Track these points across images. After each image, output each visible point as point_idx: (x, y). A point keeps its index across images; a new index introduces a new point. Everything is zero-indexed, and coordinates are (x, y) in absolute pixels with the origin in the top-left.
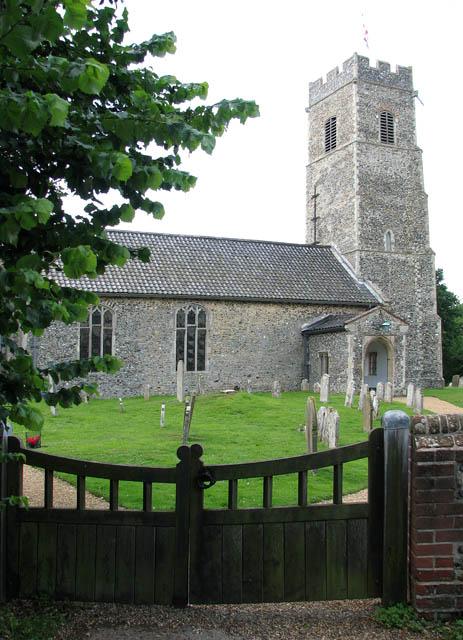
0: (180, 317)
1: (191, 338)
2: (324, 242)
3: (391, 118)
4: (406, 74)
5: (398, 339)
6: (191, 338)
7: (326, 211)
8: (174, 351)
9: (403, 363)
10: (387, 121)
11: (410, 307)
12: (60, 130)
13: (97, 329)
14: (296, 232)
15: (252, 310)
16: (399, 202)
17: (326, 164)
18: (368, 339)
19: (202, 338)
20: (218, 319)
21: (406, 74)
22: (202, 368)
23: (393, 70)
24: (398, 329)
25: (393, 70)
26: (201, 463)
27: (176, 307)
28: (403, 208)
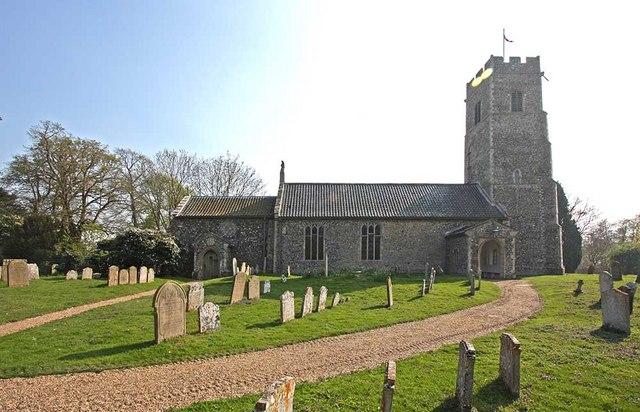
0: (364, 229)
1: (371, 242)
2: (473, 182)
3: (520, 94)
4: (534, 62)
5: (509, 241)
6: (371, 242)
7: (474, 162)
9: (512, 256)
10: (517, 96)
11: (535, 220)
12: (474, 139)
13: (315, 238)
14: (458, 177)
15: (410, 225)
16: (526, 150)
17: (477, 129)
18: (482, 241)
19: (378, 241)
20: (387, 230)
21: (534, 62)
22: (378, 257)
23: (523, 61)
24: (508, 233)
25: (523, 61)
26: (290, 291)
27: (361, 225)
28: (530, 153)
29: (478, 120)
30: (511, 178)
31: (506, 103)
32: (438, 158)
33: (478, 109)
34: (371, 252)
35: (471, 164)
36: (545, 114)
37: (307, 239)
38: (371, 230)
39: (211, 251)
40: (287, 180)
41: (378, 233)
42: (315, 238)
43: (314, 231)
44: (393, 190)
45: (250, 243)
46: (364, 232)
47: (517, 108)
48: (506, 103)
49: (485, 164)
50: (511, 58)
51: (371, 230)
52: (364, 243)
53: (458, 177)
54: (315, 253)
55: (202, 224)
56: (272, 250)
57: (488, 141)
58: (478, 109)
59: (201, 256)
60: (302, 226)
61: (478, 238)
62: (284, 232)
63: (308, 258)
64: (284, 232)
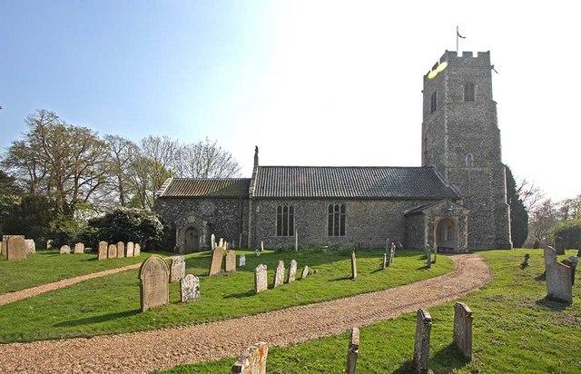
0: (331, 208)
1: (337, 219)
2: (430, 165)
3: (472, 85)
4: (485, 56)
5: (462, 218)
6: (337, 219)
7: (430, 147)
8: (327, 230)
9: (465, 233)
10: (469, 87)
11: (486, 200)
12: (430, 126)
13: (286, 216)
14: (415, 160)
15: (373, 204)
16: (478, 136)
17: (433, 117)
18: (438, 219)
19: (343, 219)
20: (351, 209)
21: (485, 56)
22: (343, 234)
23: (475, 55)
24: (461, 212)
25: (475, 55)
26: (264, 264)
27: (328, 204)
28: (481, 139)
29: (434, 109)
30: (464, 162)
31: (459, 93)
32: (397, 143)
33: (434, 99)
34: (337, 228)
35: (428, 149)
36: (495, 103)
37: (279, 217)
38: (337, 209)
39: (192, 228)
40: (260, 164)
41: (343, 211)
42: (286, 216)
43: (285, 210)
44: (357, 172)
45: (227, 220)
47: (470, 98)
48: (459, 93)
49: (441, 149)
50: (464, 53)
51: (337, 209)
52: (330, 220)
53: (415, 160)
54: (286, 230)
55: (184, 203)
56: (247, 227)
57: (443, 128)
58: (434, 99)
60: (275, 205)
61: (433, 216)
63: (279, 234)
64: (258, 211)
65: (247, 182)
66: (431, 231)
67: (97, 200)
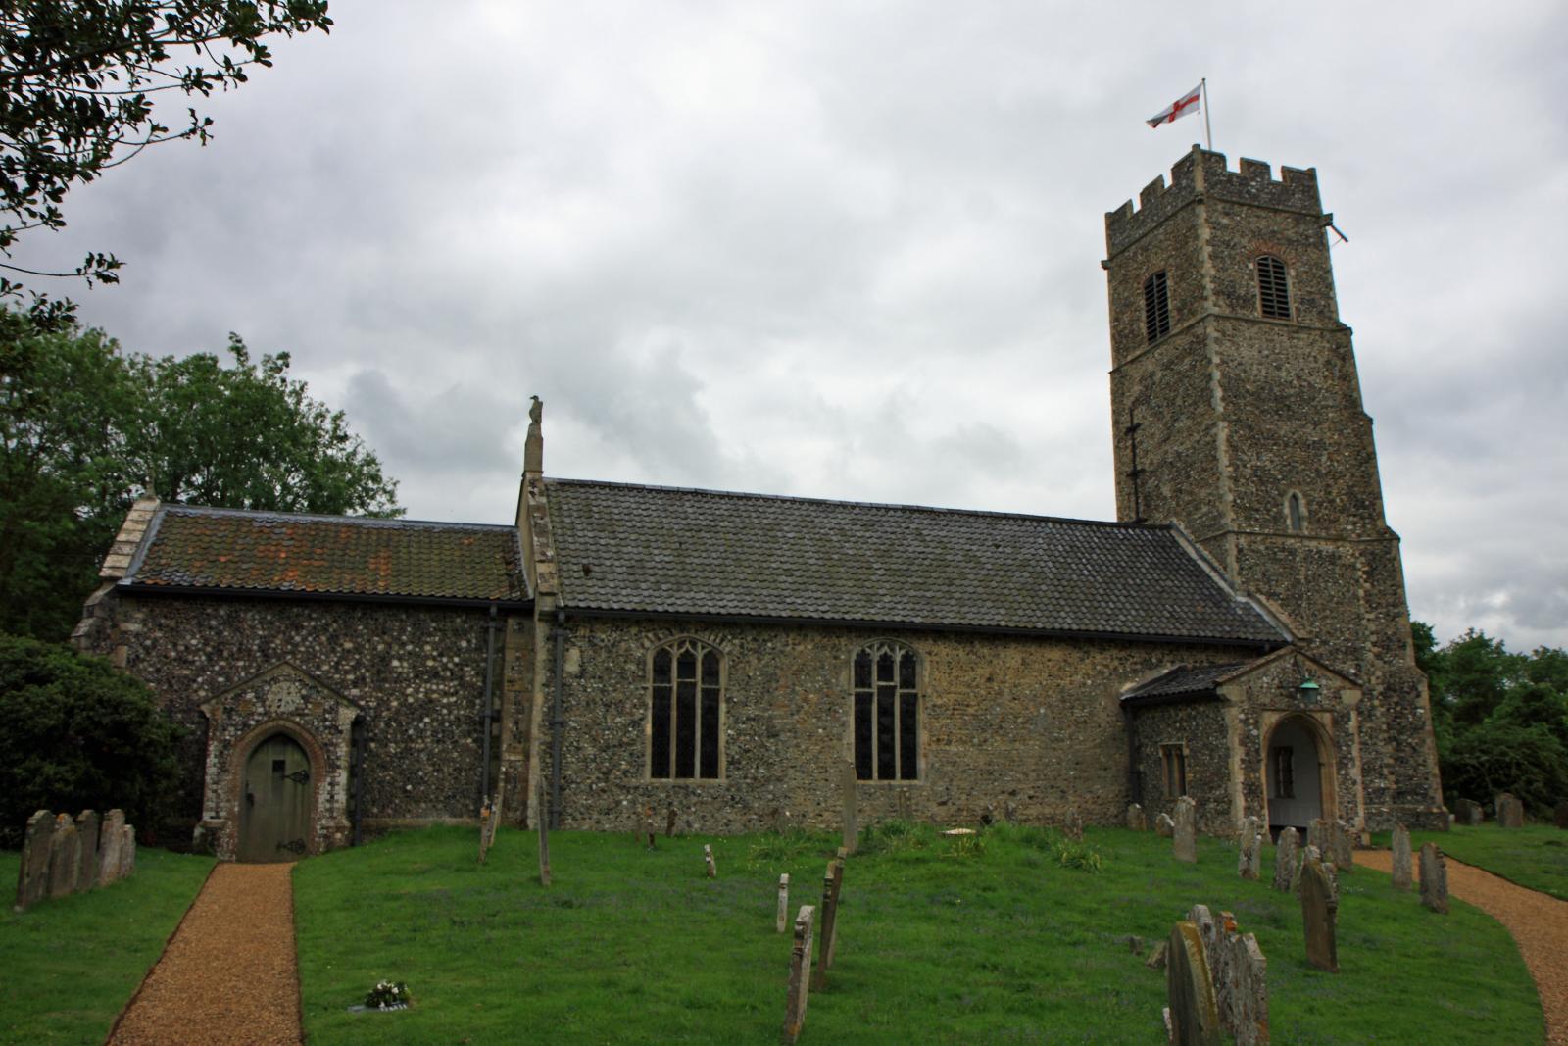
0: (862, 665)
1: (886, 711)
3: (1280, 268)
5: (1340, 721)
6: (886, 711)
10: (1272, 274)
13: (687, 690)
14: (1091, 493)
18: (1271, 719)
22: (910, 772)
24: (1337, 696)
27: (851, 649)
28: (1319, 445)
29: (1158, 327)
30: (1278, 518)
31: (1219, 276)
32: (1031, 430)
33: (1155, 292)
34: (886, 748)
35: (1144, 463)
36: (1347, 331)
37: (661, 697)
38: (885, 670)
39: (282, 738)
40: (554, 469)
41: (909, 681)
42: (687, 690)
43: (687, 665)
44: (1009, 528)
45: (428, 706)
46: (862, 680)
47: (1275, 305)
48: (1219, 276)
49: (1196, 467)
50: (1246, 163)
51: (885, 670)
52: (862, 720)
53: (1091, 493)
54: (886, 748)
55: (231, 621)
56: (522, 737)
57: (1206, 395)
58: (1155, 292)
59: (236, 757)
60: (642, 648)
61: (1257, 709)
62: (572, 667)
63: (660, 770)
64: (572, 667)
65: (497, 541)
66: (1250, 765)
67: (1478, 666)
